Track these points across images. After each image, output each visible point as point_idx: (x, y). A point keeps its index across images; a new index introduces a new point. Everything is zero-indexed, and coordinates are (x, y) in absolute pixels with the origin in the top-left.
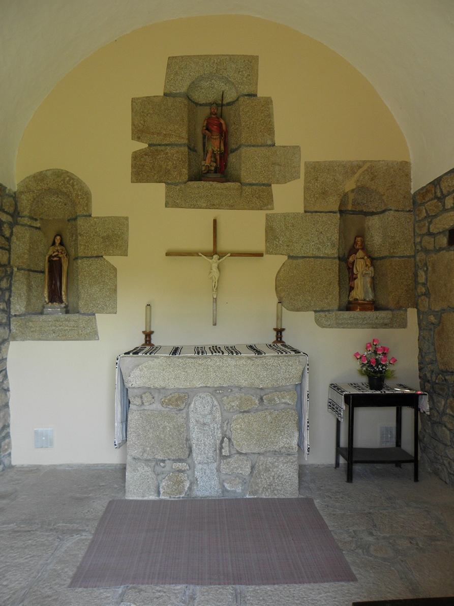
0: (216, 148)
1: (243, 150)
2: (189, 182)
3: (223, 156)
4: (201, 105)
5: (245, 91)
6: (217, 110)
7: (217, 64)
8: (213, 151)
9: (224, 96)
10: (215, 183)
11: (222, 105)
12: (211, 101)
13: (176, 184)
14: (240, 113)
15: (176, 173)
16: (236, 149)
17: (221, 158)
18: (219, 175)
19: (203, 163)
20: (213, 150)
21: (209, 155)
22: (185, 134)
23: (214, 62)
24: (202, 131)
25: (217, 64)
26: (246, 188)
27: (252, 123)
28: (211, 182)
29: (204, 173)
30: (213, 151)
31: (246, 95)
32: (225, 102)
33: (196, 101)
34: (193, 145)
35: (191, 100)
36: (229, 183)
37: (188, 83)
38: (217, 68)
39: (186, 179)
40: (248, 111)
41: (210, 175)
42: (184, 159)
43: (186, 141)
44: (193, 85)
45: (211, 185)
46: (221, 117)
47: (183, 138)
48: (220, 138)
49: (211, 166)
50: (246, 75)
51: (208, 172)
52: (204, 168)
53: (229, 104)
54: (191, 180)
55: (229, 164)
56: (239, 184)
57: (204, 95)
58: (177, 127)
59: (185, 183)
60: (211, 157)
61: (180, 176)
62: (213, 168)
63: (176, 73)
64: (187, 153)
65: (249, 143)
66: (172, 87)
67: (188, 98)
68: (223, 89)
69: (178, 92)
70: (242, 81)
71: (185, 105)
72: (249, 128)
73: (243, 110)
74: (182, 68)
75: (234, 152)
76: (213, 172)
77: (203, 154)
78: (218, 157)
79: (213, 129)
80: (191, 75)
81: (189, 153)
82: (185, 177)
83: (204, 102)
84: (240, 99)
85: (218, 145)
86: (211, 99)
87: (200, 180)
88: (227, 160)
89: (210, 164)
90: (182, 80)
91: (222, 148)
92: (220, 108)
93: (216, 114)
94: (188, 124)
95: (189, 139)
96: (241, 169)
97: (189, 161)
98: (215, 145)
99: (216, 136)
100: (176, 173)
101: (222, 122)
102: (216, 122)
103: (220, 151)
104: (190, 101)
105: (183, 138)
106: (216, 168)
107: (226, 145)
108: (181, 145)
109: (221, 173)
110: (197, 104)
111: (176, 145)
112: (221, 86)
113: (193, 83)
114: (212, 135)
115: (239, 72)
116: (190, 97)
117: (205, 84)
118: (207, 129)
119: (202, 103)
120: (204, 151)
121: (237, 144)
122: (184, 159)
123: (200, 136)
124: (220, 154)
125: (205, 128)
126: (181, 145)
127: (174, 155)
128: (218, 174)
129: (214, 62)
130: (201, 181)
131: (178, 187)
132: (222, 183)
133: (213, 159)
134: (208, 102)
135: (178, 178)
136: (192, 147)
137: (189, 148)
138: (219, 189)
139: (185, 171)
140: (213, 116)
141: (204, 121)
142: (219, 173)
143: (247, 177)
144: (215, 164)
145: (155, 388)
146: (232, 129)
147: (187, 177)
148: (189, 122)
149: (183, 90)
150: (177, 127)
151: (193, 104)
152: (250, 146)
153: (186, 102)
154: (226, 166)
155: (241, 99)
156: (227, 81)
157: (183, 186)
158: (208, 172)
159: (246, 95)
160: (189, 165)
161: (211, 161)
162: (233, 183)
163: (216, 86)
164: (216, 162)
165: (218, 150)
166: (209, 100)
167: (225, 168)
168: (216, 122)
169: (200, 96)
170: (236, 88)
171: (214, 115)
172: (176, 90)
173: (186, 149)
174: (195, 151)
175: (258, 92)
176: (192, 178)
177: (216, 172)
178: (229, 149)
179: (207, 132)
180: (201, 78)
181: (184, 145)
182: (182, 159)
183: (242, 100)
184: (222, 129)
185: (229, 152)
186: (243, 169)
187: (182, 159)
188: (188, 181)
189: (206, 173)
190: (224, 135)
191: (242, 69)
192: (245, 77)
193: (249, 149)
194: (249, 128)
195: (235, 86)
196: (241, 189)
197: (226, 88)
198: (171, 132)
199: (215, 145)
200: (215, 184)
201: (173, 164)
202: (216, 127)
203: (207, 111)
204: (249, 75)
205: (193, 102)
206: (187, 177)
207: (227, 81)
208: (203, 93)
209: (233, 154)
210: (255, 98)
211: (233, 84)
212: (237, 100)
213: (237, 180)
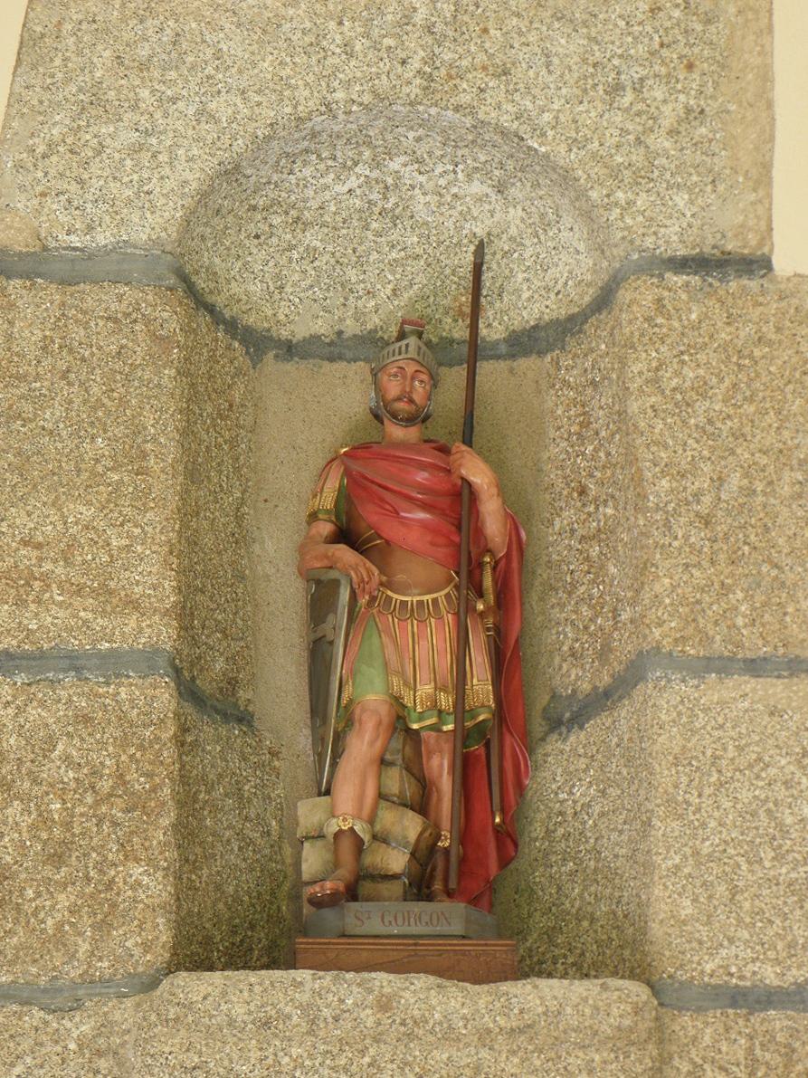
0: (425, 689)
1: (667, 703)
2: (182, 978)
3: (489, 759)
4: (290, 350)
5: (672, 231)
6: (435, 381)
7: (429, 29)
8: (399, 722)
9: (486, 277)
10: (422, 981)
11: (475, 351)
12: (374, 321)
13: (62, 999)
14: (634, 407)
15: (64, 900)
16: (603, 699)
17: (466, 769)
18: (447, 916)
19: (310, 813)
20: (397, 700)
21: (362, 746)
22: (151, 577)
23: (407, 20)
24: (302, 550)
25: (429, 29)
26: (701, 1031)
27: (735, 481)
28: (381, 979)
29: (317, 903)
30: (399, 722)
31: (682, 265)
32: (493, 329)
33: (251, 320)
34: (220, 665)
35: (211, 309)
36: (543, 983)
37: (192, 174)
38: (431, 59)
39: (161, 956)
40: (702, 390)
41: (370, 918)
42: (139, 784)
43: (160, 633)
44: (230, 192)
45: (384, 1005)
46: (468, 440)
47: (134, 604)
48: (463, 612)
49: (381, 838)
50: (669, 116)
51: (352, 893)
52: (313, 860)
53: (526, 342)
54: (202, 964)
55: (538, 830)
56: (638, 991)
57: (337, 269)
58: (88, 513)
59: (150, 984)
60: (383, 762)
61: (103, 926)
62: (397, 861)
63: (95, 103)
64: (171, 729)
65: (719, 647)
66: (51, 204)
67: (191, 289)
68: (480, 231)
69: (103, 238)
70: (638, 157)
71: (155, 337)
72: (707, 521)
73: (655, 381)
74: (143, 67)
75: (578, 720)
76: (396, 888)
77: (304, 740)
78: (441, 768)
79: (391, 530)
80: (213, 118)
81: (185, 730)
82: (146, 937)
83: (321, 327)
84: (624, 295)
85: (446, 662)
86: (379, 303)
87: (279, 956)
88: (520, 788)
89: (371, 821)
90: (137, 149)
91: (481, 685)
92: (455, 377)
93: (418, 418)
94: (184, 495)
95: (185, 616)
96: (649, 868)
97: (188, 803)
98: (413, 661)
99: (422, 581)
100: (64, 900)
101: (477, 473)
102: (422, 477)
103: (461, 710)
104: (204, 319)
105: (134, 604)
106: (425, 855)
107: (507, 661)
108: (113, 664)
109: (474, 901)
110: (257, 343)
111: (75, 663)
112: (455, 205)
113: (231, 172)
114: (388, 585)
115: (616, 89)
116: (201, 283)
117: (333, 188)
118: (345, 535)
119: (300, 331)
120: (318, 709)
121: (604, 654)
122: (139, 784)
123: (282, 596)
124: (465, 736)
125: (326, 528)
126: (113, 664)
127: (51, 742)
128: (443, 906)
129: (407, 20)
130: (291, 965)
131: (80, 1026)
132: (477, 980)
133: (395, 781)
134: (351, 327)
135: (84, 947)
136: (205, 685)
137: (189, 691)
138: (449, 1036)
139: (148, 884)
140: (397, 432)
141: (323, 474)
142: (450, 894)
143: (704, 932)
144: (410, 826)
145: (98, 283)
146: (559, 534)
147: (164, 934)
148: (193, 473)
149: (151, 225)
150: (88, 513)
151: (223, 340)
152: (721, 666)
153: (169, 317)
154: (508, 840)
155: (639, 296)
156: (515, 158)
157: (124, 1012)
158: (352, 893)
159: (682, 265)
160: (186, 833)
161: (381, 796)
162: (580, 989)
163: (420, 204)
164: (422, 804)
165: (446, 701)
166: (359, 316)
167: (504, 862)
168: (422, 477)
169: (286, 284)
170: (587, 215)
171: (410, 420)
172: (90, 228)
173: (164, 697)
174: (244, 719)
175: (777, 237)
176: (200, 949)
177: (420, 886)
178: (543, 700)
179: (344, 553)
180: (303, 139)
181: (145, 661)
182: (120, 777)
183: (648, 298)
184: (478, 531)
185: (538, 726)
186: (665, 863)
187: (120, 777)
188: (173, 967)
189: (332, 901)
190: (493, 583)
191: (637, 72)
192: (666, 123)
193: (715, 690)
194: (707, 521)
195: (582, 195)
196: (660, 1034)
197: (503, 217)
198: (27, 555)
199: (413, 661)
200: (420, 994)
201: (45, 820)
202: (421, 515)
203: (346, 395)
204: (695, 115)
205: (232, 326)
206: (165, 937)
207: (515, 158)
208: (312, 254)
209: (576, 738)
210: (753, 285)
211: (566, 178)
212: (604, 300)
213: (619, 952)
